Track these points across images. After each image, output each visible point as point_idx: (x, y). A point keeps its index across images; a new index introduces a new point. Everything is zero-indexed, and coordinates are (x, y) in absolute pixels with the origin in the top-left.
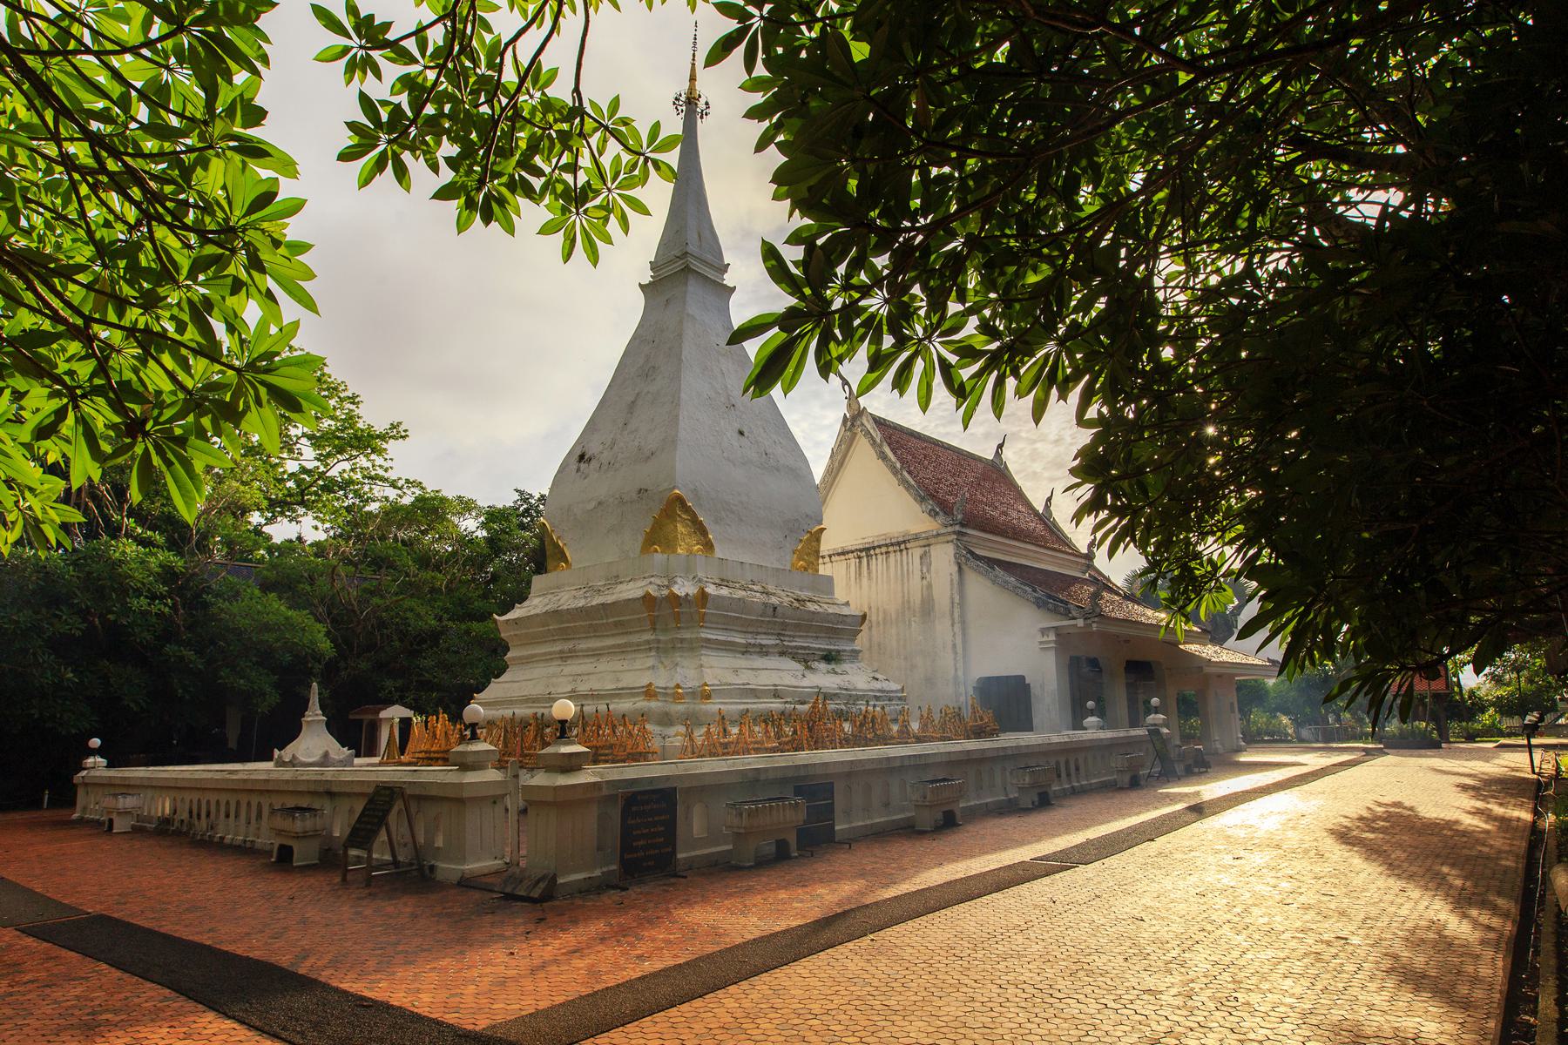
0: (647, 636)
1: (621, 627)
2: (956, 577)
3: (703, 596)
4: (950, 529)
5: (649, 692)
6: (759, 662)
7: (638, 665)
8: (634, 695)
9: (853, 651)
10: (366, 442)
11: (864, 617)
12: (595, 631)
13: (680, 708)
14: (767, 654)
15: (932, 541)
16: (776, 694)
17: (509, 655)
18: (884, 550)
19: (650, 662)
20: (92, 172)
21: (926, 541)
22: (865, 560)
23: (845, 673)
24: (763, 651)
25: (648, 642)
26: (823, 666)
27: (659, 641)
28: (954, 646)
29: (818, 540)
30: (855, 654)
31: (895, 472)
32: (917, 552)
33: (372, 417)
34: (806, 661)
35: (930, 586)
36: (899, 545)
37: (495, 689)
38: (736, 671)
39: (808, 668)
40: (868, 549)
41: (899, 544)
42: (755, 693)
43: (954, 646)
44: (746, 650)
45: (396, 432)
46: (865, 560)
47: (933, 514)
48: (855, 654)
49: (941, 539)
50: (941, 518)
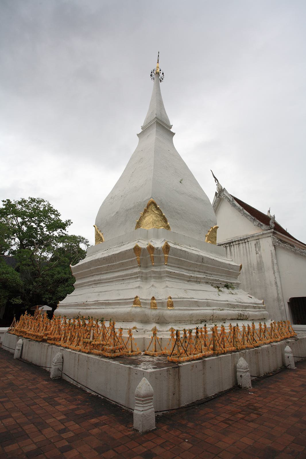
0: (137, 270)
1: (123, 266)
2: (273, 251)
3: (167, 248)
4: (269, 231)
5: (136, 302)
6: (197, 286)
7: (130, 286)
8: (127, 303)
9: (237, 283)
10: (63, 226)
11: (241, 267)
12: (109, 270)
13: (154, 312)
14: (199, 282)
15: (260, 237)
16: (208, 305)
17: (76, 283)
18: (237, 243)
19: (138, 284)
20: (177, 345)
21: (257, 238)
22: (228, 248)
23: (236, 294)
24: (198, 281)
25: (136, 273)
26: (225, 290)
27: (142, 273)
28: (276, 283)
29: (216, 232)
30: (238, 285)
31: (240, 211)
32: (253, 243)
33: (63, 219)
34: (218, 287)
35: (260, 257)
36: (245, 240)
37: (69, 299)
38: (185, 290)
39: (220, 291)
40: (230, 243)
41: (244, 239)
42: (197, 304)
43: (276, 283)
44: (190, 280)
45: (68, 223)
46: (228, 248)
47: (259, 226)
48: (238, 285)
49: (264, 236)
50: (264, 227)
